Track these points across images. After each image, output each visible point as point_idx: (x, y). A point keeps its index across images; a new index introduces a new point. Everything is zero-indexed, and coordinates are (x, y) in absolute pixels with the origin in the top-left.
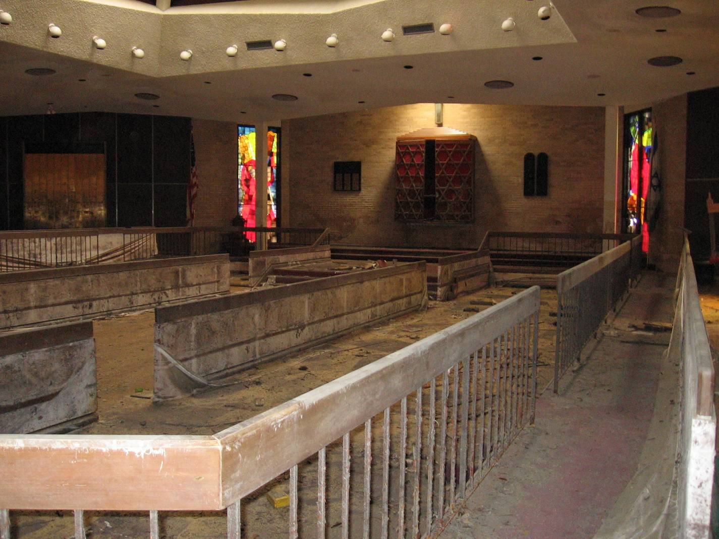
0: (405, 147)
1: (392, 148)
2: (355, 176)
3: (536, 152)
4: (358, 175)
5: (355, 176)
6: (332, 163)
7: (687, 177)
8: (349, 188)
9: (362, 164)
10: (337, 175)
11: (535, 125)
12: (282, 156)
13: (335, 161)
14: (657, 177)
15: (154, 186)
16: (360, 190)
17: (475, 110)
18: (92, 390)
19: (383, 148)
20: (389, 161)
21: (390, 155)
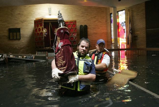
0: (38, 22)
1: (32, 23)
2: (18, 34)
3: (83, 25)
4: (19, 33)
5: (18, 34)
6: (7, 29)
7: (146, 29)
8: (12, 38)
9: (21, 29)
10: (10, 33)
11: (82, 16)
12: (122, 9)
13: (9, 28)
14: (131, 30)
15: (44, 23)
16: (20, 39)
17: (66, 8)
18: (126, 53)
19: (29, 23)
20: (32, 28)
21: (32, 25)
